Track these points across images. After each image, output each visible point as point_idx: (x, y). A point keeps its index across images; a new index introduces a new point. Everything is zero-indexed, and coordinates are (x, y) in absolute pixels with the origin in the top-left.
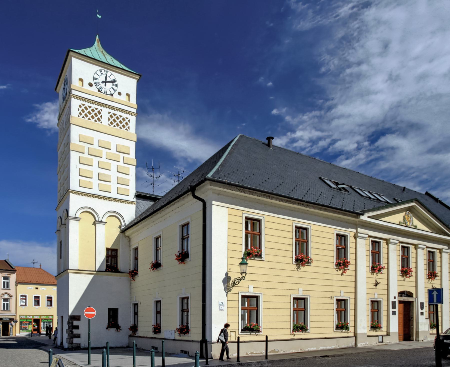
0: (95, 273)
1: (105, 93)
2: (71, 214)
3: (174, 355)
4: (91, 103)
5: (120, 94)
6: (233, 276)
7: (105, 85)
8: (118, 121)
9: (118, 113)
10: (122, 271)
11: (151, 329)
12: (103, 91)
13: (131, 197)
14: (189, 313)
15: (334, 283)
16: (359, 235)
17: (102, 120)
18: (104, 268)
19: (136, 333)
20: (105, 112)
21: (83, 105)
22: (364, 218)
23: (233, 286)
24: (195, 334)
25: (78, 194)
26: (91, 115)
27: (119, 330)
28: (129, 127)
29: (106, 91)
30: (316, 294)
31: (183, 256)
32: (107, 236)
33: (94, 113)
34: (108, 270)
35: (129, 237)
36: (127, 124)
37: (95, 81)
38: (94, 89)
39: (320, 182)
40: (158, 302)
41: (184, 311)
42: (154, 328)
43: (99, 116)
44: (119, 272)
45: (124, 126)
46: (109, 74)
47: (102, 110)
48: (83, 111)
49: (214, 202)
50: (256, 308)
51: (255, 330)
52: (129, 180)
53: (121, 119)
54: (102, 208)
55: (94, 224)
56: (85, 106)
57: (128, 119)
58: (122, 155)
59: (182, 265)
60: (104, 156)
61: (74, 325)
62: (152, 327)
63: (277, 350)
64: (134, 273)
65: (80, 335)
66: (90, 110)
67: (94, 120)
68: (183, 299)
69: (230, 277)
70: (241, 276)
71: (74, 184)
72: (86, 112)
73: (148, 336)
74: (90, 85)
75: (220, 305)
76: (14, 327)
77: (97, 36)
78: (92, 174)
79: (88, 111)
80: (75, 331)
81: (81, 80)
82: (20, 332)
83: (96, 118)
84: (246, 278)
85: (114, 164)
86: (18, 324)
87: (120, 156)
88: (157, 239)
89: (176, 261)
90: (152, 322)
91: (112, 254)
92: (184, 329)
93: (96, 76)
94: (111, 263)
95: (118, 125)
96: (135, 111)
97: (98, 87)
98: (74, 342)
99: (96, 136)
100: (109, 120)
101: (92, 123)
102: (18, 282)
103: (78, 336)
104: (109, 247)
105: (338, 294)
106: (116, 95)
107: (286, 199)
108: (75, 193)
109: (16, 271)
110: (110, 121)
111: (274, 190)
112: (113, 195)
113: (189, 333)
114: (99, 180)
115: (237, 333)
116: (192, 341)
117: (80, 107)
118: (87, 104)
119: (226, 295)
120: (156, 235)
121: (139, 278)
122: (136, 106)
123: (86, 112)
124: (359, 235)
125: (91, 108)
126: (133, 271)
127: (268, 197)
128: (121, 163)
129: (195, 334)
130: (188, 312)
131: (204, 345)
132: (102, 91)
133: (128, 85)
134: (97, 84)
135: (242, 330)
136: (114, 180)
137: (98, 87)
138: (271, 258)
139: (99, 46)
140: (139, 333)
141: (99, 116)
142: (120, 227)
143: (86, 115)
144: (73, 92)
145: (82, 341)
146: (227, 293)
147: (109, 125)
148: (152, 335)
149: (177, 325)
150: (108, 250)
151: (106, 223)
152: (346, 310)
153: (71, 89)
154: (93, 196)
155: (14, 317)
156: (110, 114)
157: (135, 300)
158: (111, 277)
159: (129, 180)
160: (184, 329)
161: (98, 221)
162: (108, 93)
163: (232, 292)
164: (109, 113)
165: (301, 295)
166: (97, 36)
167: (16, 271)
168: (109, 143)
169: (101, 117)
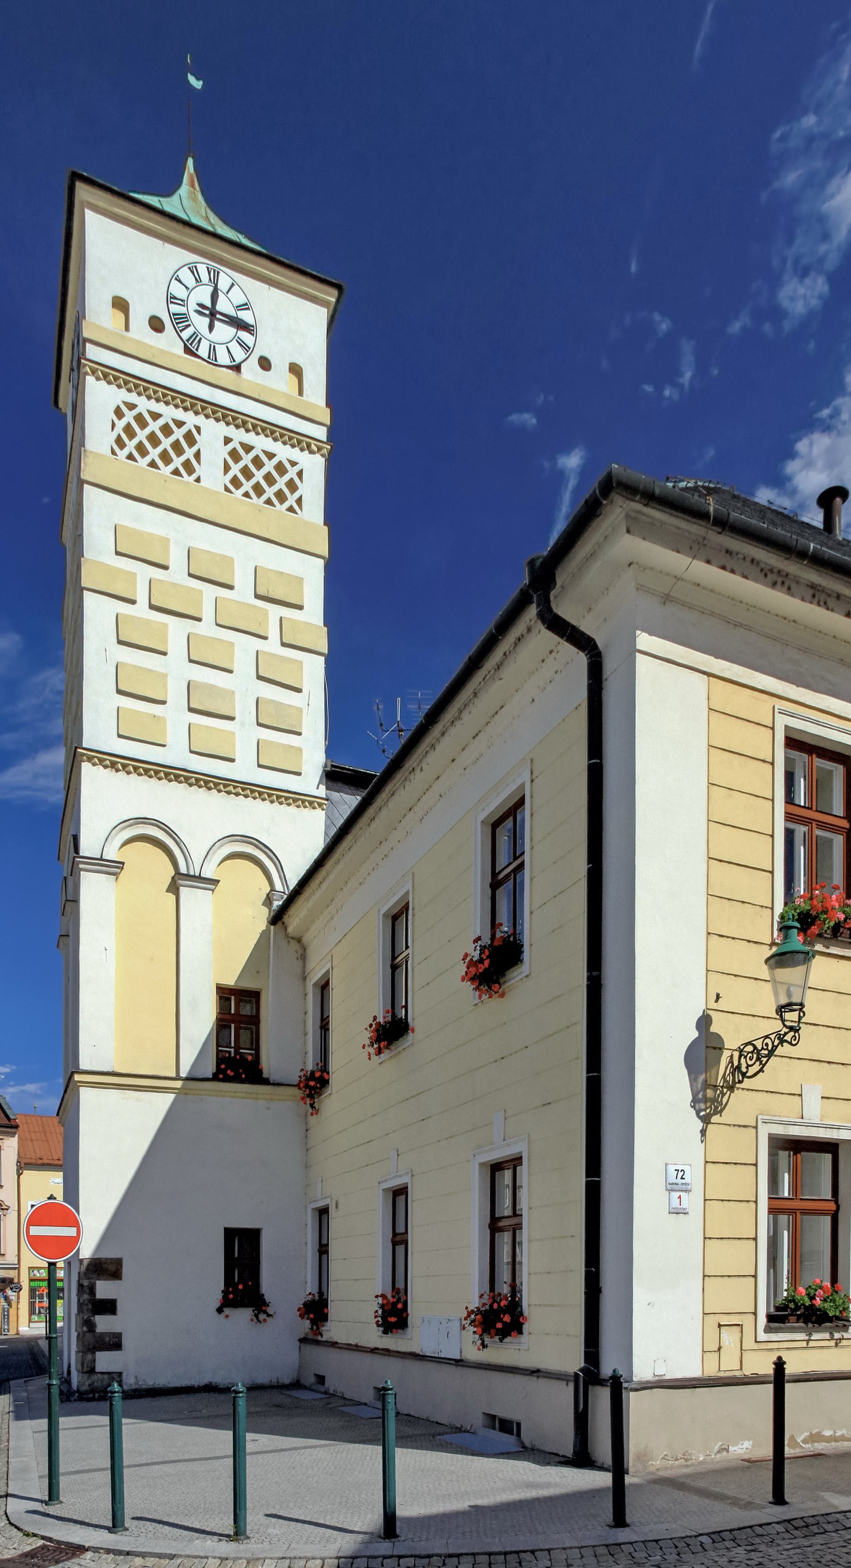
0: (178, 1084)
1: (212, 360)
2: (89, 846)
3: (458, 1438)
4: (158, 400)
5: (265, 364)
6: (733, 1034)
7: (211, 327)
8: (259, 476)
9: (262, 443)
10: (273, 1078)
11: (371, 1309)
12: (203, 351)
13: (311, 782)
14: (524, 1236)
17: (200, 470)
18: (210, 1068)
19: (323, 1329)
21: (131, 407)
23: (731, 1088)
24: (551, 1338)
25: (113, 765)
26: (160, 449)
27: (262, 1316)
28: (299, 501)
29: (212, 350)
31: (497, 963)
32: (220, 936)
33: (172, 439)
34: (224, 1072)
35: (299, 940)
36: (292, 486)
37: (174, 309)
38: (169, 343)
40: (399, 1193)
41: (501, 1225)
42: (382, 1306)
44: (266, 1082)
45: (281, 496)
46: (224, 282)
47: (198, 429)
48: (129, 431)
49: (644, 640)
50: (832, 1206)
51: (830, 1319)
52: (300, 710)
53: (269, 466)
54: (202, 822)
55: (174, 888)
56: (135, 412)
57: (297, 469)
58: (275, 612)
59: (493, 1003)
60: (208, 613)
62: (374, 1306)
64: (315, 1084)
65: (119, 1336)
66: (154, 426)
67: (171, 467)
68: (496, 1168)
69: (718, 1037)
70: (777, 1026)
71: (99, 729)
72: (142, 435)
73: (363, 1343)
75: (671, 1188)
76: (14, 1304)
77: (190, 162)
78: (165, 686)
79: (147, 431)
80: (103, 1323)
81: (121, 305)
82: (30, 1321)
83: (178, 462)
85: (244, 649)
86: (25, 1294)
87: (266, 613)
88: (398, 917)
89: (469, 986)
90: (376, 1282)
91: (238, 1008)
92: (500, 1317)
93: (178, 290)
94: (237, 1048)
95: (258, 490)
96: (321, 433)
97: (186, 335)
100: (227, 468)
101: (162, 482)
102: (23, 1161)
103: (114, 1343)
104: (230, 980)
108: (101, 761)
109: (17, 1127)
110: (230, 475)
112: (244, 769)
113: (520, 1332)
114: (191, 710)
116: (536, 1372)
117: (119, 413)
118: (144, 405)
119: (703, 1132)
120: (390, 903)
121: (333, 1100)
122: (325, 416)
123: (142, 435)
125: (161, 422)
126: (313, 1073)
128: (272, 646)
129: (551, 1338)
130: (516, 1229)
131: (602, 1397)
132: (200, 353)
133: (294, 326)
134: (180, 321)
135: (771, 1318)
136: (244, 710)
137: (186, 335)
139: (195, 200)
140: (333, 1331)
141: (189, 453)
142: (268, 901)
143: (141, 449)
144: (92, 352)
145: (126, 1364)
146: (706, 1120)
147: (227, 489)
148: (374, 1337)
149: (472, 1294)
150: (224, 994)
151: (216, 882)
153: (86, 340)
154: (167, 775)
155: (12, 1274)
156: (230, 446)
157: (319, 1196)
158: (237, 1097)
159: (300, 710)
160: (500, 1317)
161: (188, 876)
162: (223, 358)
163: (727, 1116)
164: (227, 441)
166: (190, 162)
167: (17, 1127)
168: (227, 562)
169: (197, 455)
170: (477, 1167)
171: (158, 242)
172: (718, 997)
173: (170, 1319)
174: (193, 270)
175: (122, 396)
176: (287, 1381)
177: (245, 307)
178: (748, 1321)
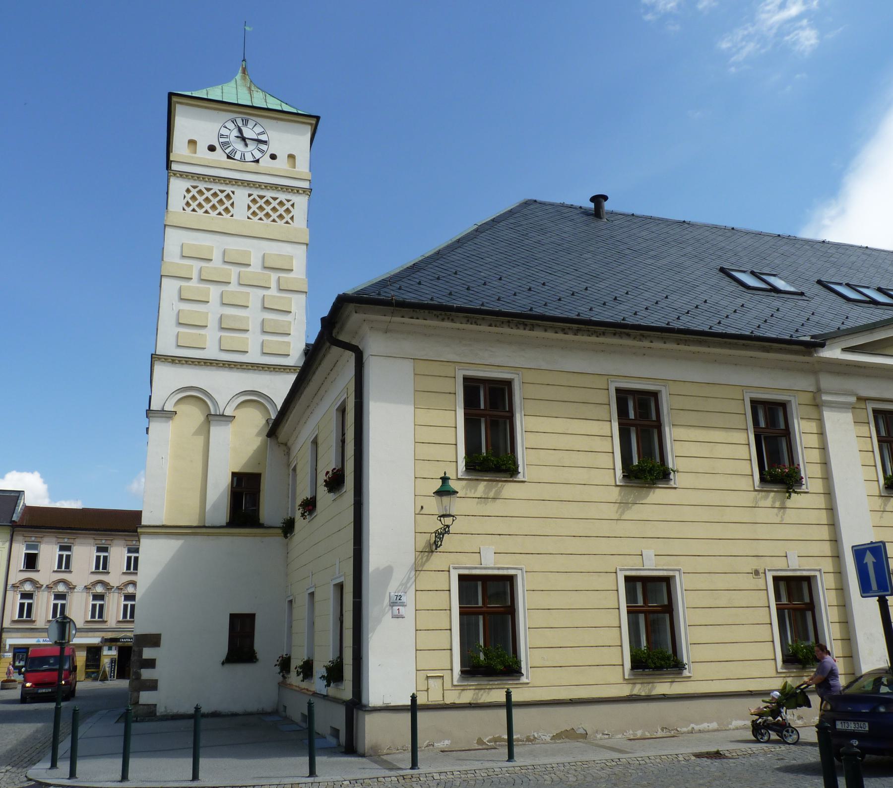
1: (243, 160)
12: (238, 156)
15: (762, 532)
16: (825, 398)
20: (241, 196)
22: (833, 353)
30: (703, 564)
35: (286, 444)
36: (288, 211)
37: (222, 140)
38: (219, 156)
39: (725, 282)
43: (228, 204)
47: (233, 193)
48: (194, 198)
52: (290, 322)
54: (224, 387)
57: (291, 203)
58: (274, 276)
60: (234, 279)
61: (144, 657)
63: (581, 731)
65: (156, 681)
74: (212, 148)
84: (452, 530)
85: (255, 297)
91: (245, 489)
98: (141, 701)
99: (215, 245)
101: (213, 220)
103: (152, 685)
104: (236, 470)
105: (780, 564)
106: (266, 161)
107: (575, 326)
111: (597, 309)
115: (447, 679)
118: (202, 186)
124: (825, 398)
127: (522, 327)
128: (273, 292)
137: (227, 151)
138: (546, 474)
152: (811, 607)
156: (252, 198)
158: (243, 542)
162: (249, 158)
165: (651, 567)
170: (332, 588)
172: (422, 507)
173: (186, 673)
175: (187, 184)
176: (269, 710)
178: (447, 674)
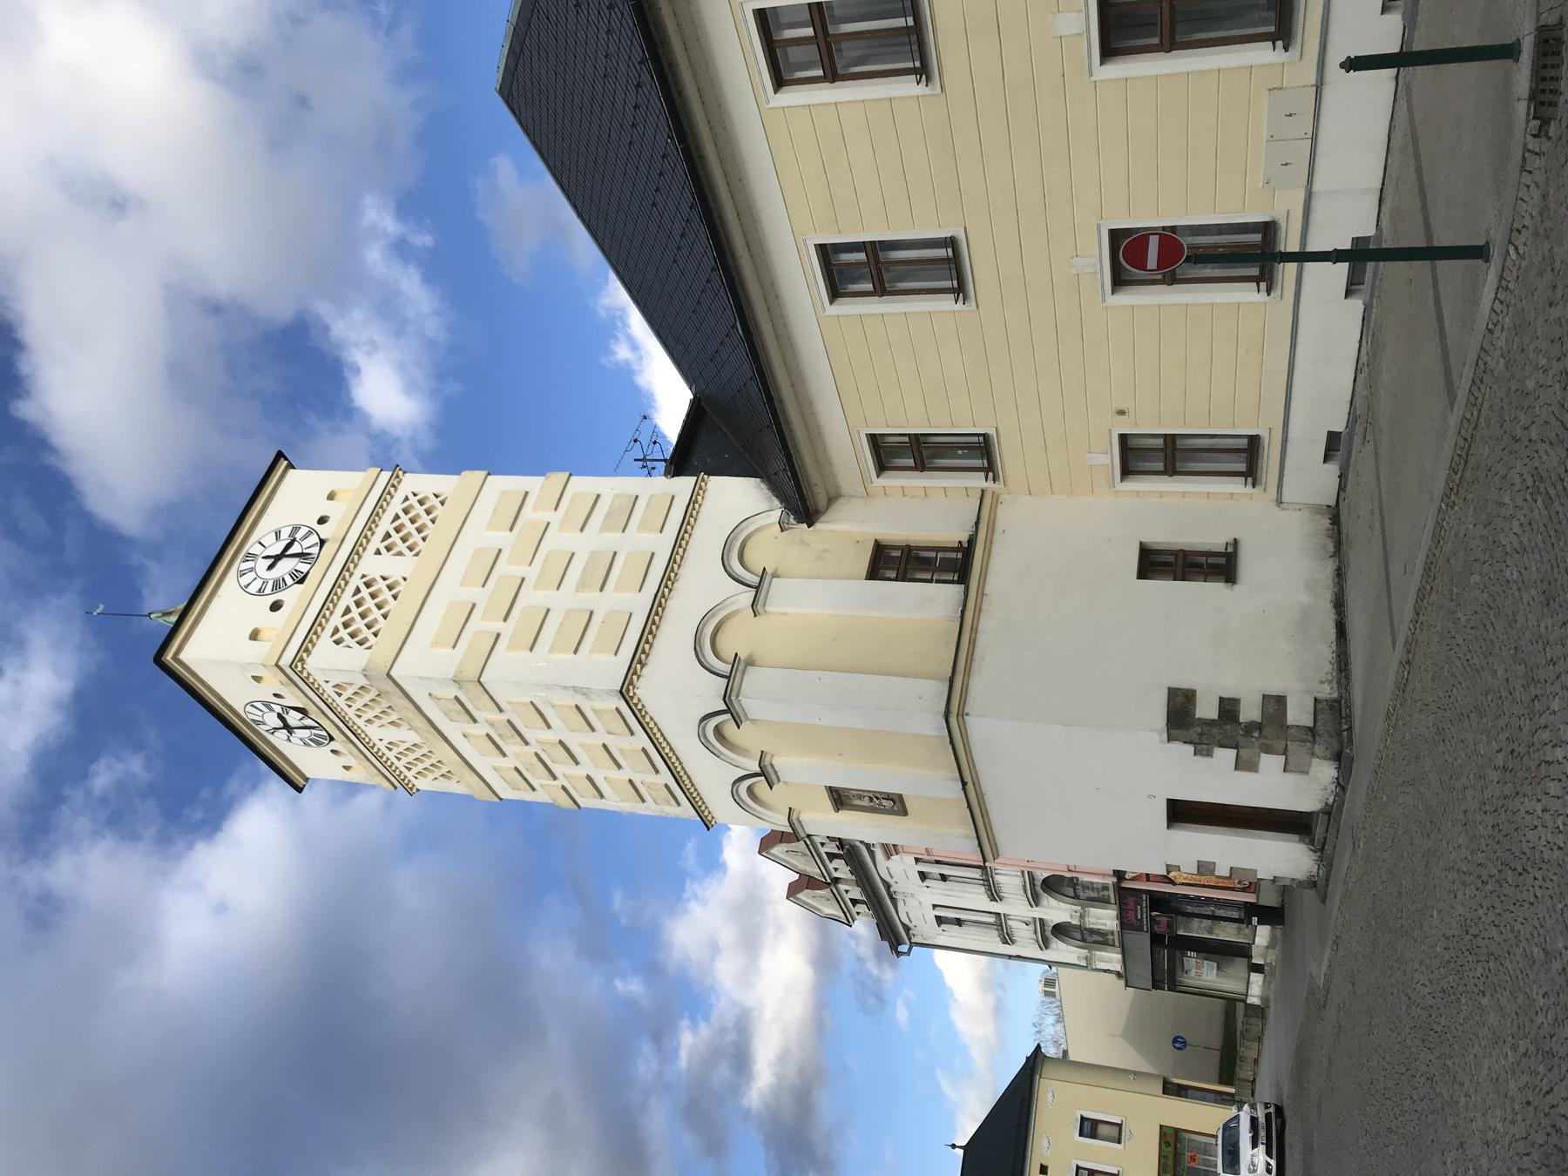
5: (322, 521)
37: (268, 590)
38: (292, 596)
44: (972, 541)
93: (254, 588)
118: (336, 620)
122: (474, 477)
134: (278, 585)
137: (289, 581)
156: (383, 550)
164: (378, 552)
171: (216, 600)
174: (242, 574)
175: (325, 639)
177: (278, 534)
